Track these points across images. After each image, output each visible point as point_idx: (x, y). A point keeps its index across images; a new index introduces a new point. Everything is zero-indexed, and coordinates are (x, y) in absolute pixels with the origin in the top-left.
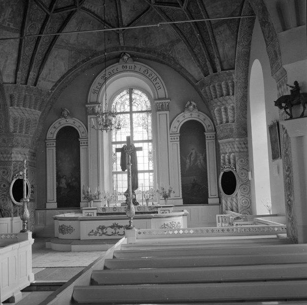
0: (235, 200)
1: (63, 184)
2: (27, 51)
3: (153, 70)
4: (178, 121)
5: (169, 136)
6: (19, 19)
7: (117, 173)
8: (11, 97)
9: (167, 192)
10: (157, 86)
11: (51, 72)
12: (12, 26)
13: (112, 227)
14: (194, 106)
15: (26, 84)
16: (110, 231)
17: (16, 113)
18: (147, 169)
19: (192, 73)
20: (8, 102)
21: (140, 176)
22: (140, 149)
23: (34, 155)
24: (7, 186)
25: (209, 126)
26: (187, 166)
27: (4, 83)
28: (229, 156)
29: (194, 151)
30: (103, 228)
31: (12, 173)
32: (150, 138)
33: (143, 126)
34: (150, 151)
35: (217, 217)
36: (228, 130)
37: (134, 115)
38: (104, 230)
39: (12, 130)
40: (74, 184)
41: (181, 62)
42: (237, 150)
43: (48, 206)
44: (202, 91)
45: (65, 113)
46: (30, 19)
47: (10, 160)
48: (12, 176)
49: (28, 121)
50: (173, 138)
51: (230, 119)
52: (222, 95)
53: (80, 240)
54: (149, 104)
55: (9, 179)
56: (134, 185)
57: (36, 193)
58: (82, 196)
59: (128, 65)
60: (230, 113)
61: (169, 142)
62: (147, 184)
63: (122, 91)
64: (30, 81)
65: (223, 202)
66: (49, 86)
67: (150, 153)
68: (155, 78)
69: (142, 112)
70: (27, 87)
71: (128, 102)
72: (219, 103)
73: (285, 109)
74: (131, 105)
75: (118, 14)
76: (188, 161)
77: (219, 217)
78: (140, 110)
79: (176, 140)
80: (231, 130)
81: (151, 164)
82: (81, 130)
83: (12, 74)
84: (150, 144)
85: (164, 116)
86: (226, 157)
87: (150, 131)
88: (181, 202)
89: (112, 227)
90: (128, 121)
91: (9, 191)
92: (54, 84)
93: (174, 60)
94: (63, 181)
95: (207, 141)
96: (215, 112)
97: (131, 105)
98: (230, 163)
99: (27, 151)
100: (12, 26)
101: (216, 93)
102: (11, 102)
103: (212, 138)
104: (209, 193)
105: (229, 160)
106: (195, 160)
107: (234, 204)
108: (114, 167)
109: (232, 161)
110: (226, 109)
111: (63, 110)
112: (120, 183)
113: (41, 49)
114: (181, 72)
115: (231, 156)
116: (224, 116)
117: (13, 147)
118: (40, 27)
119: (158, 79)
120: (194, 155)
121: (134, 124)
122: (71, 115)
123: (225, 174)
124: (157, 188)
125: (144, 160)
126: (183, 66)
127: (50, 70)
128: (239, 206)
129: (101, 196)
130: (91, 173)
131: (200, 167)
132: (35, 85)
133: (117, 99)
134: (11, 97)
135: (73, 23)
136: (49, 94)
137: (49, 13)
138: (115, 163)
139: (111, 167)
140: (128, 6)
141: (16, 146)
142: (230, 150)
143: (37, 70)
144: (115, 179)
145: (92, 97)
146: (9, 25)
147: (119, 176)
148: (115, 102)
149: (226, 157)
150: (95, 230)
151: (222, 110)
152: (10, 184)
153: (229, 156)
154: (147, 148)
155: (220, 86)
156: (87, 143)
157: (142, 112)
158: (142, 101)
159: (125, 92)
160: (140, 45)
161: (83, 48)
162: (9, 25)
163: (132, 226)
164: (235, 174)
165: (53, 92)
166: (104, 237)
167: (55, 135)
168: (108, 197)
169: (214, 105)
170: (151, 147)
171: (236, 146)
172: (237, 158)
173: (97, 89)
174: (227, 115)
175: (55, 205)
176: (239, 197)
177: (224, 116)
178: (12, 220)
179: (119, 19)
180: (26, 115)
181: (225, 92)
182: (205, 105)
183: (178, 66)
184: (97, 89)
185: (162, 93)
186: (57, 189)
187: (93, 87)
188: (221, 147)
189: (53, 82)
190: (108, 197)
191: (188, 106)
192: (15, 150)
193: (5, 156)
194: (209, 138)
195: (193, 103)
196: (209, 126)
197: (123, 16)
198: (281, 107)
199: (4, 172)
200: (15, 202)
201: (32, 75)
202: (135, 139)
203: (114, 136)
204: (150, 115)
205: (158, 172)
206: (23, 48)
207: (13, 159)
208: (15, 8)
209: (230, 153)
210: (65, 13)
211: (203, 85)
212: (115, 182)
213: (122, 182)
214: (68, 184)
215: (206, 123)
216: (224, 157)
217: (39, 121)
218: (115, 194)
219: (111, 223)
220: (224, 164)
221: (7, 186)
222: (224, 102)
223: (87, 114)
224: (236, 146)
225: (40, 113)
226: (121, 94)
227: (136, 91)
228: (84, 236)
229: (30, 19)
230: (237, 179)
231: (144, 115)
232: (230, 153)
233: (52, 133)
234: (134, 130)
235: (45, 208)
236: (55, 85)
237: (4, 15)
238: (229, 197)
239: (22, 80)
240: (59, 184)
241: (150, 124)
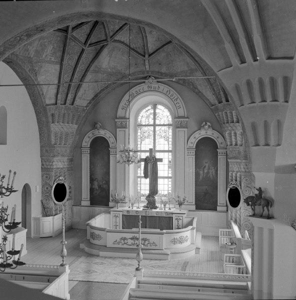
0: (238, 212)
1: (96, 186)
2: (66, 78)
3: (174, 91)
4: (195, 138)
5: (186, 150)
6: (59, 54)
7: (141, 177)
8: (53, 115)
9: (182, 200)
10: (177, 105)
11: (86, 92)
12: (53, 59)
13: (132, 239)
14: (209, 127)
15: (65, 104)
16: (130, 242)
17: (57, 129)
18: (166, 175)
19: (209, 98)
20: (50, 119)
21: (160, 181)
22: (161, 160)
23: (71, 160)
24: (49, 188)
25: (222, 143)
26: (201, 177)
27: (47, 105)
28: (236, 174)
29: (207, 165)
30: (125, 239)
31: (54, 178)
32: (170, 149)
33: (164, 138)
34: (170, 160)
35: (220, 232)
36: (236, 152)
37: (157, 128)
38: (126, 241)
39: (53, 143)
40: (105, 186)
41: (199, 87)
42: (243, 170)
43: (83, 203)
44: (216, 114)
45: (98, 126)
46: (68, 53)
47: (52, 167)
48: (53, 182)
49: (67, 134)
50: (189, 152)
51: (239, 143)
52: (233, 122)
53: (106, 246)
54: (170, 119)
55: (51, 184)
56: (154, 190)
57: (73, 192)
58: (111, 198)
59: (153, 85)
60: (239, 138)
61: (186, 156)
62: (166, 188)
63: (148, 106)
64: (68, 102)
65: (229, 211)
66: (85, 103)
67: (170, 162)
68: (176, 98)
69: (164, 125)
70: (66, 107)
71: (152, 116)
72: (230, 128)
73: (251, 206)
74: (154, 119)
75: (144, 43)
76: (201, 172)
77: (221, 231)
78: (162, 123)
79: (192, 154)
80: (239, 153)
81: (170, 172)
82: (111, 140)
83: (53, 97)
84: (170, 154)
85: (183, 133)
86: (234, 174)
87: (170, 143)
88: (194, 207)
89: (132, 239)
90: (152, 133)
91: (51, 193)
92: (89, 102)
93: (193, 85)
94: (96, 183)
95: (219, 157)
96: (226, 135)
97: (154, 119)
98: (236, 181)
99: (66, 159)
100: (53, 59)
101: (227, 118)
102: (53, 119)
103: (223, 154)
104: (218, 202)
105: (236, 177)
106: (208, 173)
107: (238, 215)
108: (139, 172)
109: (238, 179)
110: (235, 133)
111: (96, 123)
112: (143, 187)
113: (77, 76)
114: (199, 94)
115: (238, 175)
116: (233, 140)
117: (54, 156)
118: (77, 58)
119: (178, 100)
120: (207, 167)
121: (156, 136)
122: (103, 128)
123: (231, 189)
124: (174, 196)
125: (163, 169)
126: (200, 90)
127: (85, 91)
128: (242, 218)
129: (127, 200)
130: (118, 174)
131: (212, 178)
132: (73, 104)
133: (143, 113)
134: (53, 115)
135: (105, 52)
136: (84, 110)
137: (84, 48)
138: (139, 169)
139: (136, 172)
140: (154, 37)
141: (57, 156)
142: (237, 170)
143: (74, 92)
144: (139, 183)
145: (120, 113)
146: (50, 59)
147: (143, 180)
148: (141, 115)
149: (234, 174)
150: (118, 240)
151: (233, 134)
152: (52, 187)
153: (236, 174)
154: (166, 157)
155: (232, 113)
156: (116, 152)
157: (164, 125)
158: (164, 115)
159: (150, 107)
160: (164, 70)
161: (114, 71)
162: (50, 59)
163: (140, 268)
164: (240, 189)
165: (88, 108)
166: (125, 246)
167: (89, 144)
168: (132, 201)
169: (226, 129)
170: (170, 157)
171: (242, 167)
172: (242, 177)
173: (125, 106)
174: (236, 139)
175: (88, 203)
176: (242, 211)
177: (233, 140)
178: (53, 219)
179: (146, 48)
180: (65, 129)
181: (235, 120)
182: (219, 126)
183: (196, 90)
184: (125, 106)
185: (181, 112)
186: (90, 189)
187: (122, 104)
188: (230, 166)
189: (88, 100)
190: (132, 201)
191: (203, 126)
192: (55, 159)
193: (48, 163)
194: (221, 154)
195: (209, 124)
196: (222, 143)
197: (149, 45)
198: (248, 205)
199: (47, 177)
200: (56, 202)
201: (70, 97)
202: (157, 149)
203: (139, 146)
204: (171, 128)
205: (175, 178)
206: (62, 76)
207: (55, 167)
208: (55, 45)
209: (237, 172)
210: (98, 47)
211: (217, 109)
212: (139, 185)
213: (144, 186)
214: (100, 186)
215: (219, 141)
216: (232, 174)
217: (76, 133)
218: (138, 195)
219: (131, 235)
220: (232, 180)
221: (49, 188)
222: (234, 128)
223: (116, 127)
224: (242, 167)
225: (76, 126)
226: (147, 109)
227: (159, 107)
228: (110, 244)
229: (68, 53)
230: (241, 193)
231: (166, 128)
232: (237, 172)
233: (87, 142)
234: (157, 141)
235: (80, 205)
236: (90, 103)
237: (47, 51)
238: (234, 210)
239: (61, 101)
240: (92, 185)
241: (171, 137)
